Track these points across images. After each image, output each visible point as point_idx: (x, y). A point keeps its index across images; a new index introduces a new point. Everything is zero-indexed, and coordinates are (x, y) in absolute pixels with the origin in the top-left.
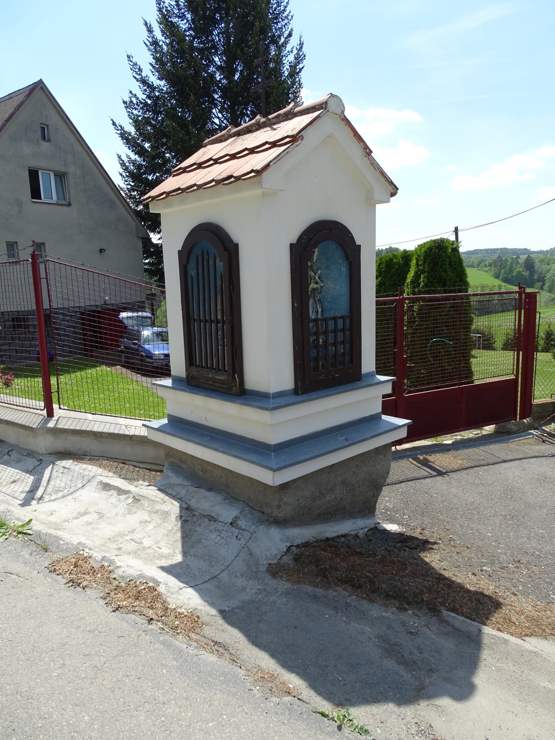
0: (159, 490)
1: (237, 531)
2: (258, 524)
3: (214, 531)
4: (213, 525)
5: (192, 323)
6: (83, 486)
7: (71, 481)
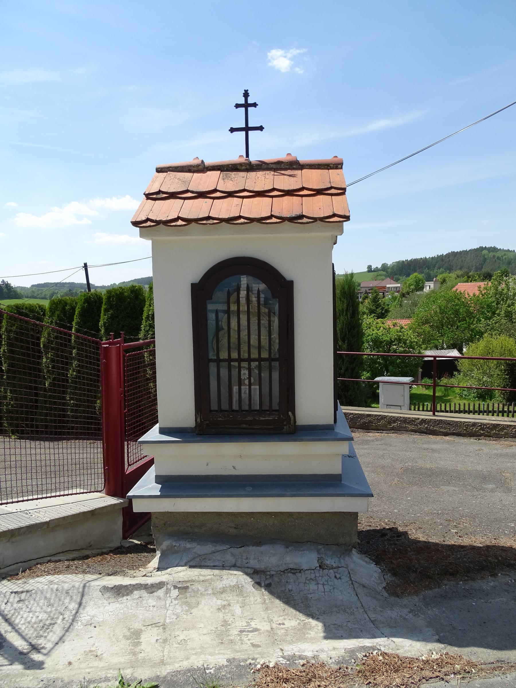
0: (191, 567)
1: (331, 571)
2: (342, 557)
3: (307, 582)
4: (302, 577)
5: (213, 368)
6: (80, 604)
7: (50, 605)
